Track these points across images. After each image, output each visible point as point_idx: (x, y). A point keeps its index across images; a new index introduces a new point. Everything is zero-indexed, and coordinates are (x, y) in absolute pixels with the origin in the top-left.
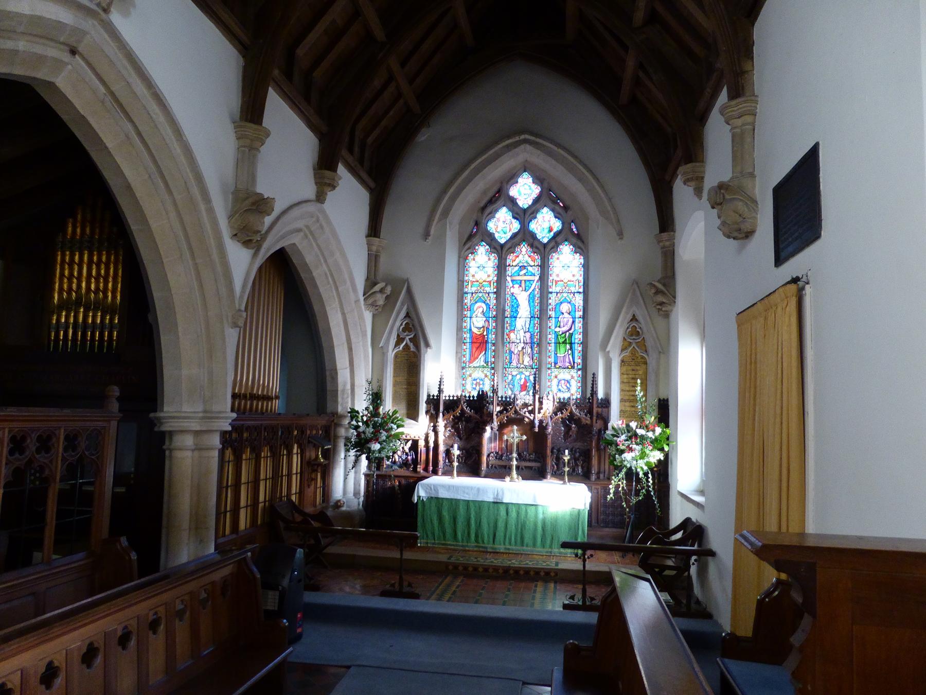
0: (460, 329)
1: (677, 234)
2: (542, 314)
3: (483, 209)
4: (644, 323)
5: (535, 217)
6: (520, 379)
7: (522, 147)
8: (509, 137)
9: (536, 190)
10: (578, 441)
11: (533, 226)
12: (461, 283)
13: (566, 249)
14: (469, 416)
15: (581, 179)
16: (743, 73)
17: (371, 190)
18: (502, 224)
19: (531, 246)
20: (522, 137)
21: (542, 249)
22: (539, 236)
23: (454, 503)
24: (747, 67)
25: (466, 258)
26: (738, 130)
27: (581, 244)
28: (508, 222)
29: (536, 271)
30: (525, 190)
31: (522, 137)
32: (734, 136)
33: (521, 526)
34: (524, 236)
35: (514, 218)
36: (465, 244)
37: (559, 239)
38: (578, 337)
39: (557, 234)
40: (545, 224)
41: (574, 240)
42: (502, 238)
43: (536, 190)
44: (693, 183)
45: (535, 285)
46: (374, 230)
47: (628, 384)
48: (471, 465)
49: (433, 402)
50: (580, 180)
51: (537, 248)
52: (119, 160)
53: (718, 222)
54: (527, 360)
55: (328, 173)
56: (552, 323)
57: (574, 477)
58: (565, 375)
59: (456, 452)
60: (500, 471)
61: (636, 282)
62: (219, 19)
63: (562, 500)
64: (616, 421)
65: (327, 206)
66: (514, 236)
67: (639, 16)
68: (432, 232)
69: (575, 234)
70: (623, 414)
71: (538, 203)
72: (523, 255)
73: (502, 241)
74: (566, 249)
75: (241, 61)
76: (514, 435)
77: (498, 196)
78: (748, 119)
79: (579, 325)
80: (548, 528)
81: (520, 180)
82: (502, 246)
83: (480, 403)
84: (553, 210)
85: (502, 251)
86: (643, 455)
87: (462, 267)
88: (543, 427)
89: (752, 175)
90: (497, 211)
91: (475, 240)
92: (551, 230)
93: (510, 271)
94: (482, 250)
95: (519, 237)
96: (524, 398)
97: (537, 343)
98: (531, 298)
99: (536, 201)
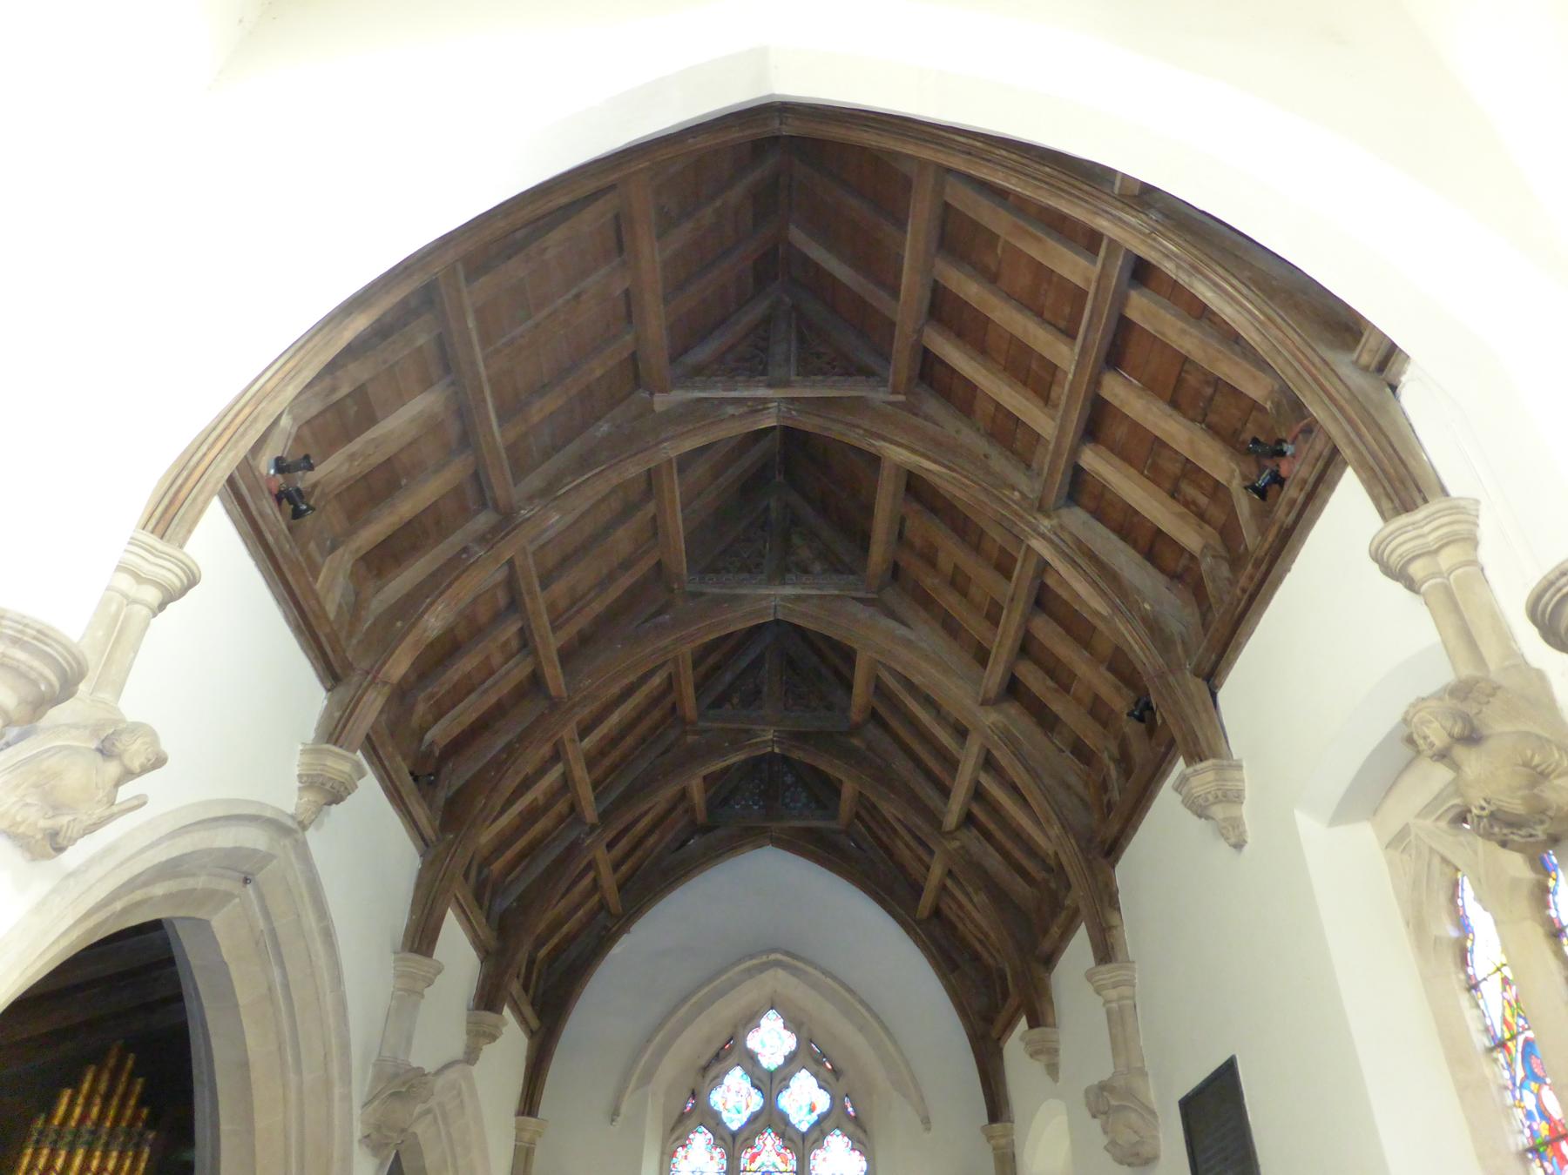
1: (1015, 1126)
3: (705, 1069)
5: (787, 1087)
7: (771, 972)
8: (752, 957)
9: (789, 1042)
11: (785, 1102)
13: (837, 1143)
16: (1110, 928)
17: (532, 1034)
18: (734, 1098)
19: (781, 1135)
20: (773, 957)
21: (799, 1141)
22: (793, 1120)
24: (1114, 920)
25: (673, 1154)
26: (1114, 1005)
27: (861, 1135)
28: (744, 1092)
30: (771, 1040)
31: (773, 957)
32: (1109, 1013)
34: (770, 1119)
35: (754, 1086)
36: (673, 1129)
37: (826, 1125)
39: (823, 1118)
40: (804, 1098)
41: (850, 1127)
42: (734, 1121)
43: (789, 1042)
44: (1044, 1058)
46: (529, 1103)
50: (861, 1029)
51: (791, 1140)
52: (245, 1021)
53: (1104, 1140)
55: (488, 1016)
62: (410, 813)
65: (476, 1070)
66: (754, 1118)
67: (952, 818)
68: (624, 1109)
71: (792, 1062)
72: (769, 1151)
73: (734, 1126)
74: (837, 1143)
75: (417, 863)
77: (729, 1050)
78: (1125, 990)
81: (763, 1021)
82: (734, 1135)
84: (815, 1075)
85: (733, 1143)
89: (1143, 1073)
90: (726, 1073)
91: (690, 1123)
92: (812, 1109)
94: (701, 1140)
95: (762, 1120)
99: (791, 1059)
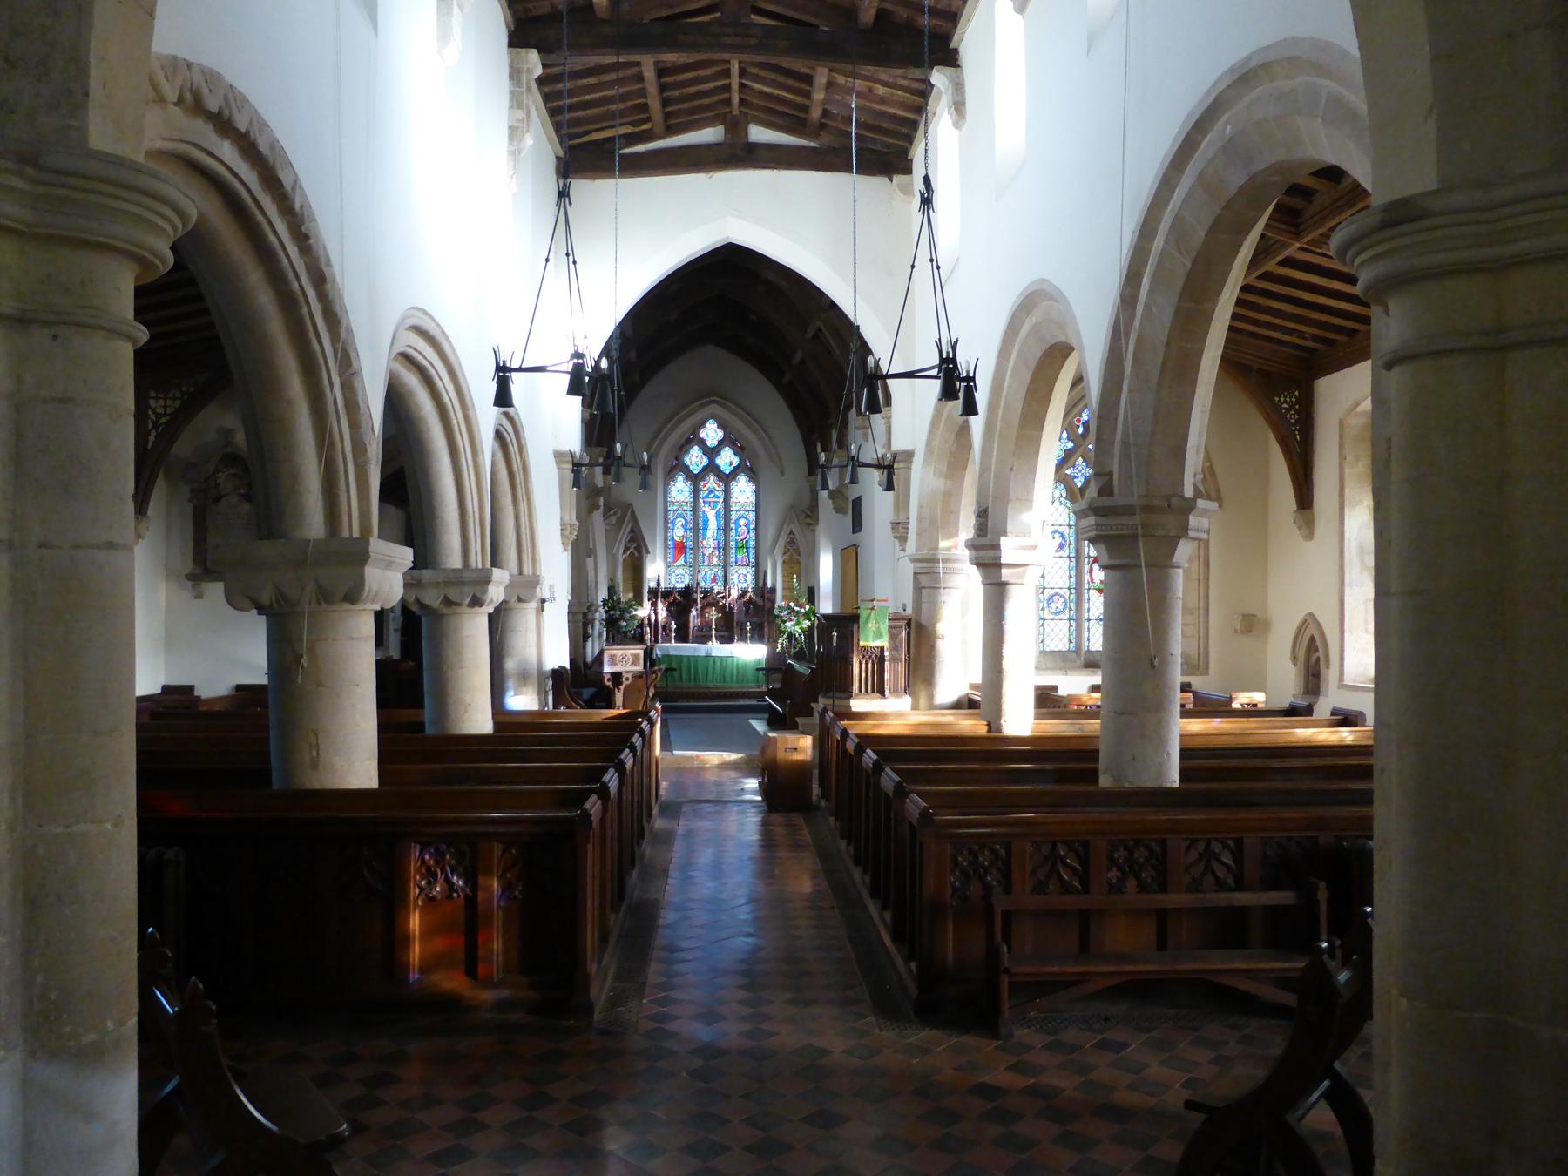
0: (666, 538)
2: (725, 528)
3: (681, 448)
4: (798, 536)
6: (710, 575)
9: (720, 434)
10: (755, 615)
11: (718, 461)
12: (666, 502)
14: (681, 601)
15: (754, 431)
18: (695, 459)
23: (680, 658)
27: (753, 476)
29: (722, 495)
30: (712, 433)
33: (723, 670)
34: (712, 468)
38: (752, 543)
40: (727, 459)
43: (720, 434)
45: (720, 505)
47: (787, 577)
48: (683, 636)
49: (654, 593)
54: (715, 560)
56: (733, 533)
57: (753, 640)
58: (743, 571)
59: (674, 626)
60: (704, 638)
61: (792, 507)
63: (749, 653)
64: (780, 602)
69: (748, 467)
70: (784, 598)
71: (721, 443)
72: (711, 482)
76: (713, 615)
77: (693, 439)
79: (752, 534)
80: (741, 670)
83: (687, 592)
85: (695, 479)
86: (798, 623)
87: (666, 492)
88: (731, 609)
93: (702, 495)
94: (680, 478)
96: (718, 588)
97: (723, 548)
98: (717, 515)
99: (720, 442)
